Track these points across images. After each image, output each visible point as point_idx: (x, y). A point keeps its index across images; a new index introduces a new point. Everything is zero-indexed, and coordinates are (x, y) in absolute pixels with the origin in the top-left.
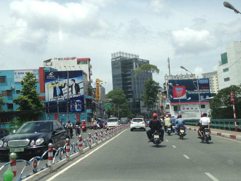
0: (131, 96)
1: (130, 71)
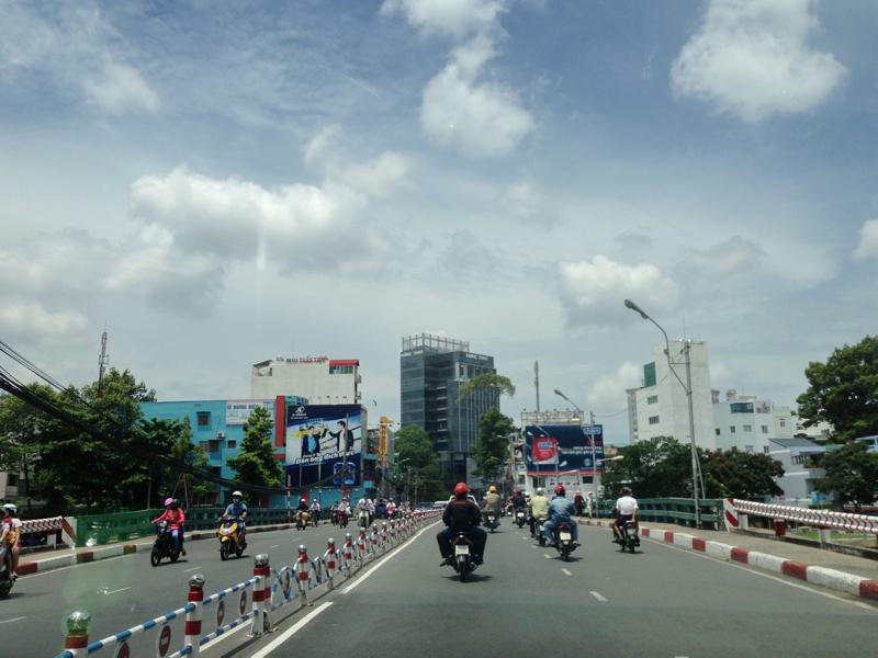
0: (444, 446)
1: (445, 382)
